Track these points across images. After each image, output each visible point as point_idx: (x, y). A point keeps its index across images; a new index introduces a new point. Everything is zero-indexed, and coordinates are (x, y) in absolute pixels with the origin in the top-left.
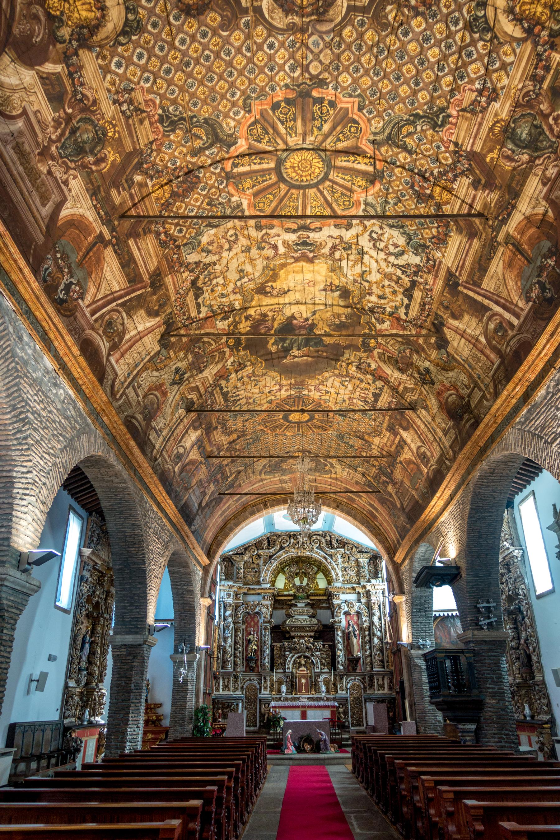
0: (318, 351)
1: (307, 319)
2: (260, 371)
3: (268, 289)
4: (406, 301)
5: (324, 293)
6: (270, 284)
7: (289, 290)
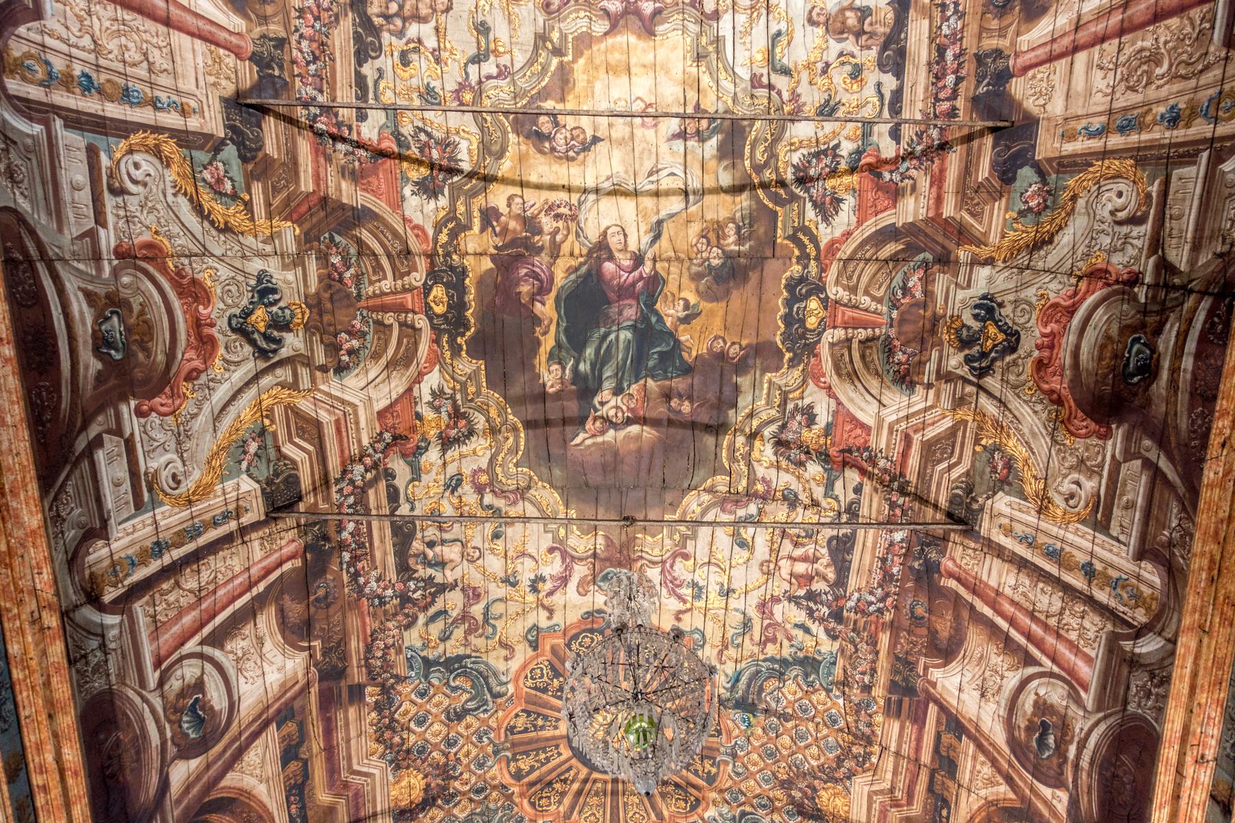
0: (667, 396)
2: (513, 473)
3: (545, 124)
4: (890, 83)
5: (679, 145)
7: (596, 140)
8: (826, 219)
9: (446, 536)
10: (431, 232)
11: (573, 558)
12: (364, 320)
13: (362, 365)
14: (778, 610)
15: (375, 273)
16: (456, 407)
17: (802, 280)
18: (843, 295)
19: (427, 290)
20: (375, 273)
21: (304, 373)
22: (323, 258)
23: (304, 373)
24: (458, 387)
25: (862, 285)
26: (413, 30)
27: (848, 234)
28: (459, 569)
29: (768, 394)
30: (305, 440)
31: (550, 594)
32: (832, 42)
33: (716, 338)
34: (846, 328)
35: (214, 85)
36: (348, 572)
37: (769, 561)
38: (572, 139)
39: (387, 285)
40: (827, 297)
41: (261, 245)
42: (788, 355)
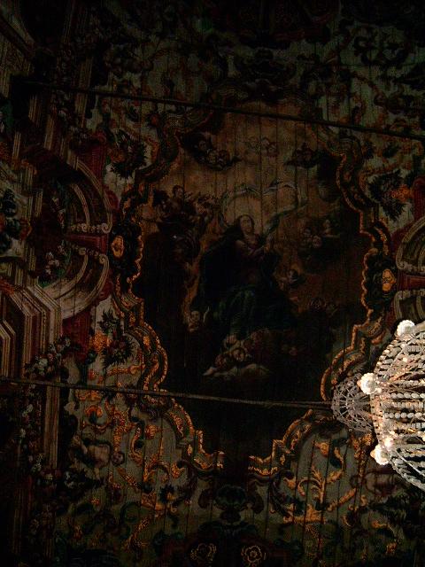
1: (261, 239)
5: (291, 169)
6: (207, 134)
7: (236, 160)
8: (393, 218)
9: (100, 438)
10: (120, 199)
11: (197, 472)
12: (66, 247)
13: (58, 281)
14: (364, 518)
15: (79, 217)
16: (119, 331)
17: (379, 257)
18: (407, 266)
19: (111, 238)
20: (79, 217)
21: (19, 273)
22: (47, 199)
23: (19, 273)
24: (123, 315)
25: (421, 259)
26: (128, 75)
27: (409, 226)
28: (106, 469)
29: (356, 341)
30: (10, 324)
31: (176, 504)
32: (390, 114)
33: (317, 299)
34: (411, 290)
35: (10, 67)
36: (22, 448)
37: (358, 476)
38: (220, 157)
39: (84, 227)
40: (397, 269)
41: (11, 173)
42: (370, 311)
